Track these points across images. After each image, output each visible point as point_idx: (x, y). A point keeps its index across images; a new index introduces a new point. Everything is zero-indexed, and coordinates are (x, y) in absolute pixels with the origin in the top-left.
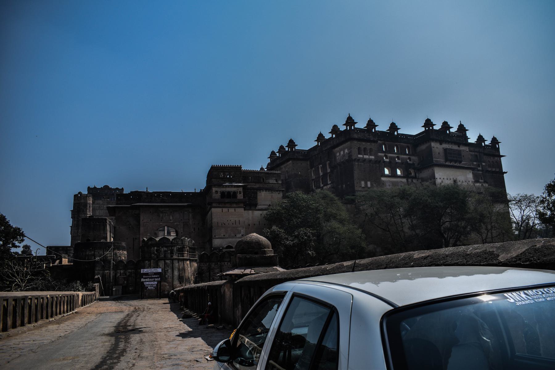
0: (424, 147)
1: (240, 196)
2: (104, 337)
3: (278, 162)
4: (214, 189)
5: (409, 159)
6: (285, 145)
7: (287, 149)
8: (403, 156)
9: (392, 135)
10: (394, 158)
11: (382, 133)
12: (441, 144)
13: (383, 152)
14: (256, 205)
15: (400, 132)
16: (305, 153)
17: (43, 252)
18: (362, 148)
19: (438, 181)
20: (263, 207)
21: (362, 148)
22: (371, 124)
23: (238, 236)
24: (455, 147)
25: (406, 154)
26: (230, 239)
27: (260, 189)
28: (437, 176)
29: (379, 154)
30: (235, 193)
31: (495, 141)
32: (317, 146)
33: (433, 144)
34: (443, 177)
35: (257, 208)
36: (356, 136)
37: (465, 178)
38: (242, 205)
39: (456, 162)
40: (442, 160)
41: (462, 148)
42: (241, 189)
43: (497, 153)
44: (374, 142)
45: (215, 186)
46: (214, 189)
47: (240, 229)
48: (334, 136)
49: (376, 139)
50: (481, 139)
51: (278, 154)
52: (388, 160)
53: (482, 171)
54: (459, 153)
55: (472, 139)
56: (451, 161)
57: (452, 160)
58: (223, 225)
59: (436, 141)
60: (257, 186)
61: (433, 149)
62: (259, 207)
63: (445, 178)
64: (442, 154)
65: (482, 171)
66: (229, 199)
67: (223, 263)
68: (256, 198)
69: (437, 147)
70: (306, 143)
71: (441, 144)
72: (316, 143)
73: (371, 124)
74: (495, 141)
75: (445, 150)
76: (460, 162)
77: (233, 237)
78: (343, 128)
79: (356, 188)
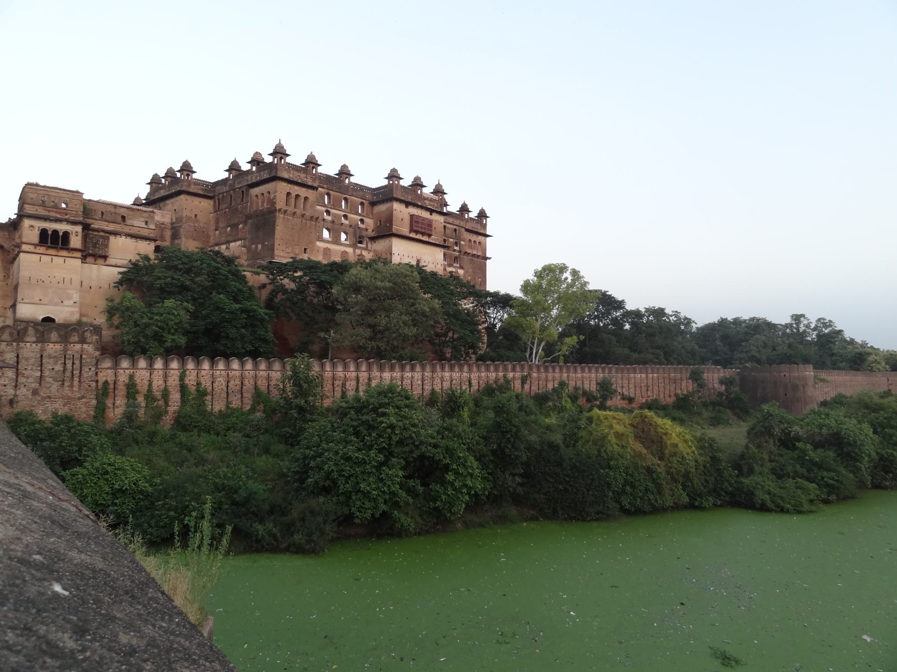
0: (383, 208)
1: (76, 241)
2: (147, 383)
3: (163, 193)
4: (27, 222)
5: (362, 221)
6: (177, 167)
7: (178, 175)
8: (352, 216)
9: (340, 182)
10: (339, 217)
11: (328, 178)
12: (407, 206)
13: (325, 206)
14: (105, 257)
15: (352, 180)
16: (207, 186)
17: (15, 216)
18: (293, 195)
19: (396, 260)
20: (119, 262)
21: (293, 195)
22: (311, 162)
23: (65, 303)
24: (425, 214)
25: (357, 213)
26: (52, 307)
27: (115, 234)
28: (395, 250)
29: (318, 207)
30: (66, 235)
31: (482, 215)
32: (226, 180)
33: (396, 206)
34: (403, 252)
35: (107, 263)
36: (285, 175)
37: (433, 259)
38: (79, 255)
39: (423, 234)
40: (405, 231)
41: (436, 217)
42: (79, 229)
43: (482, 231)
44: (314, 188)
45: (30, 216)
46: (27, 222)
47: (70, 292)
48: (254, 169)
49: (316, 185)
50: (464, 209)
51: (163, 181)
52: (329, 218)
53: (460, 252)
54: (430, 224)
55: (453, 207)
56: (417, 232)
57: (420, 232)
58: (40, 282)
59: (401, 201)
60: (111, 227)
61: (394, 212)
62: (110, 261)
63: (406, 255)
64: (407, 221)
65: (460, 252)
66: (53, 241)
67: (22, 344)
68: (107, 246)
69: (401, 212)
70: (210, 171)
71: (407, 206)
72: (226, 175)
73: (311, 162)
74: (482, 215)
75: (412, 216)
76: (430, 236)
77: (56, 304)
78: (268, 159)
79: (276, 252)
